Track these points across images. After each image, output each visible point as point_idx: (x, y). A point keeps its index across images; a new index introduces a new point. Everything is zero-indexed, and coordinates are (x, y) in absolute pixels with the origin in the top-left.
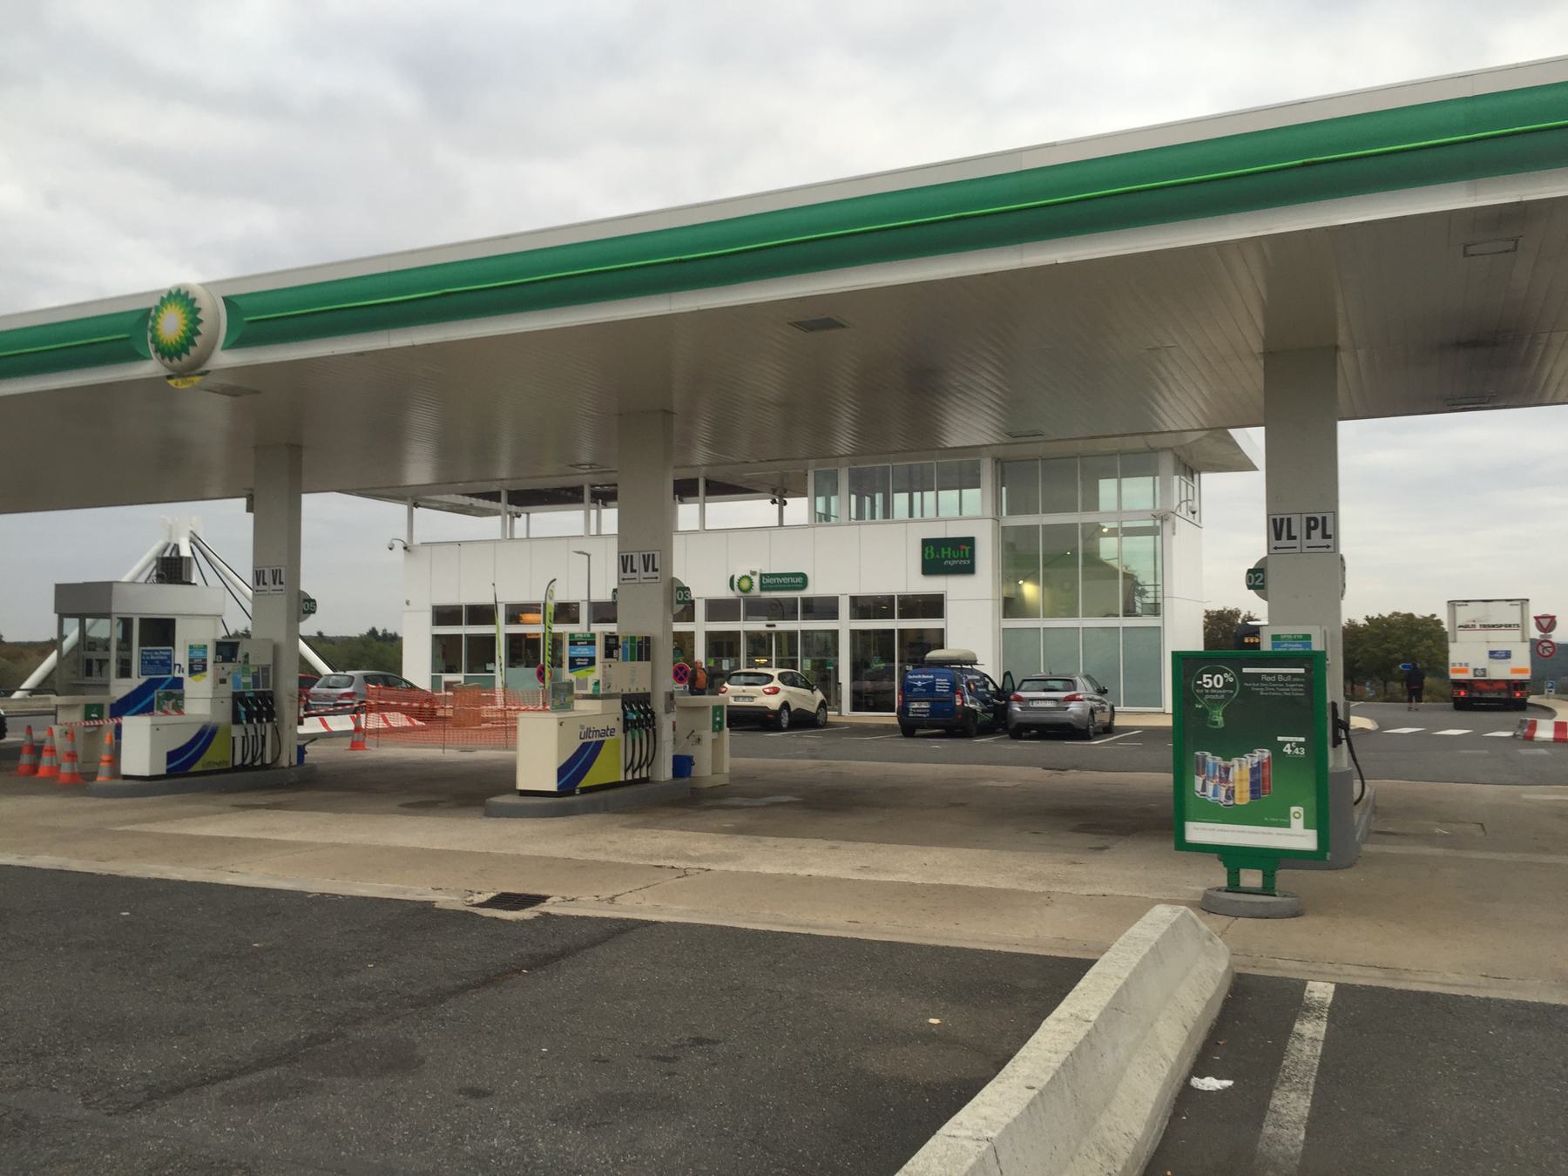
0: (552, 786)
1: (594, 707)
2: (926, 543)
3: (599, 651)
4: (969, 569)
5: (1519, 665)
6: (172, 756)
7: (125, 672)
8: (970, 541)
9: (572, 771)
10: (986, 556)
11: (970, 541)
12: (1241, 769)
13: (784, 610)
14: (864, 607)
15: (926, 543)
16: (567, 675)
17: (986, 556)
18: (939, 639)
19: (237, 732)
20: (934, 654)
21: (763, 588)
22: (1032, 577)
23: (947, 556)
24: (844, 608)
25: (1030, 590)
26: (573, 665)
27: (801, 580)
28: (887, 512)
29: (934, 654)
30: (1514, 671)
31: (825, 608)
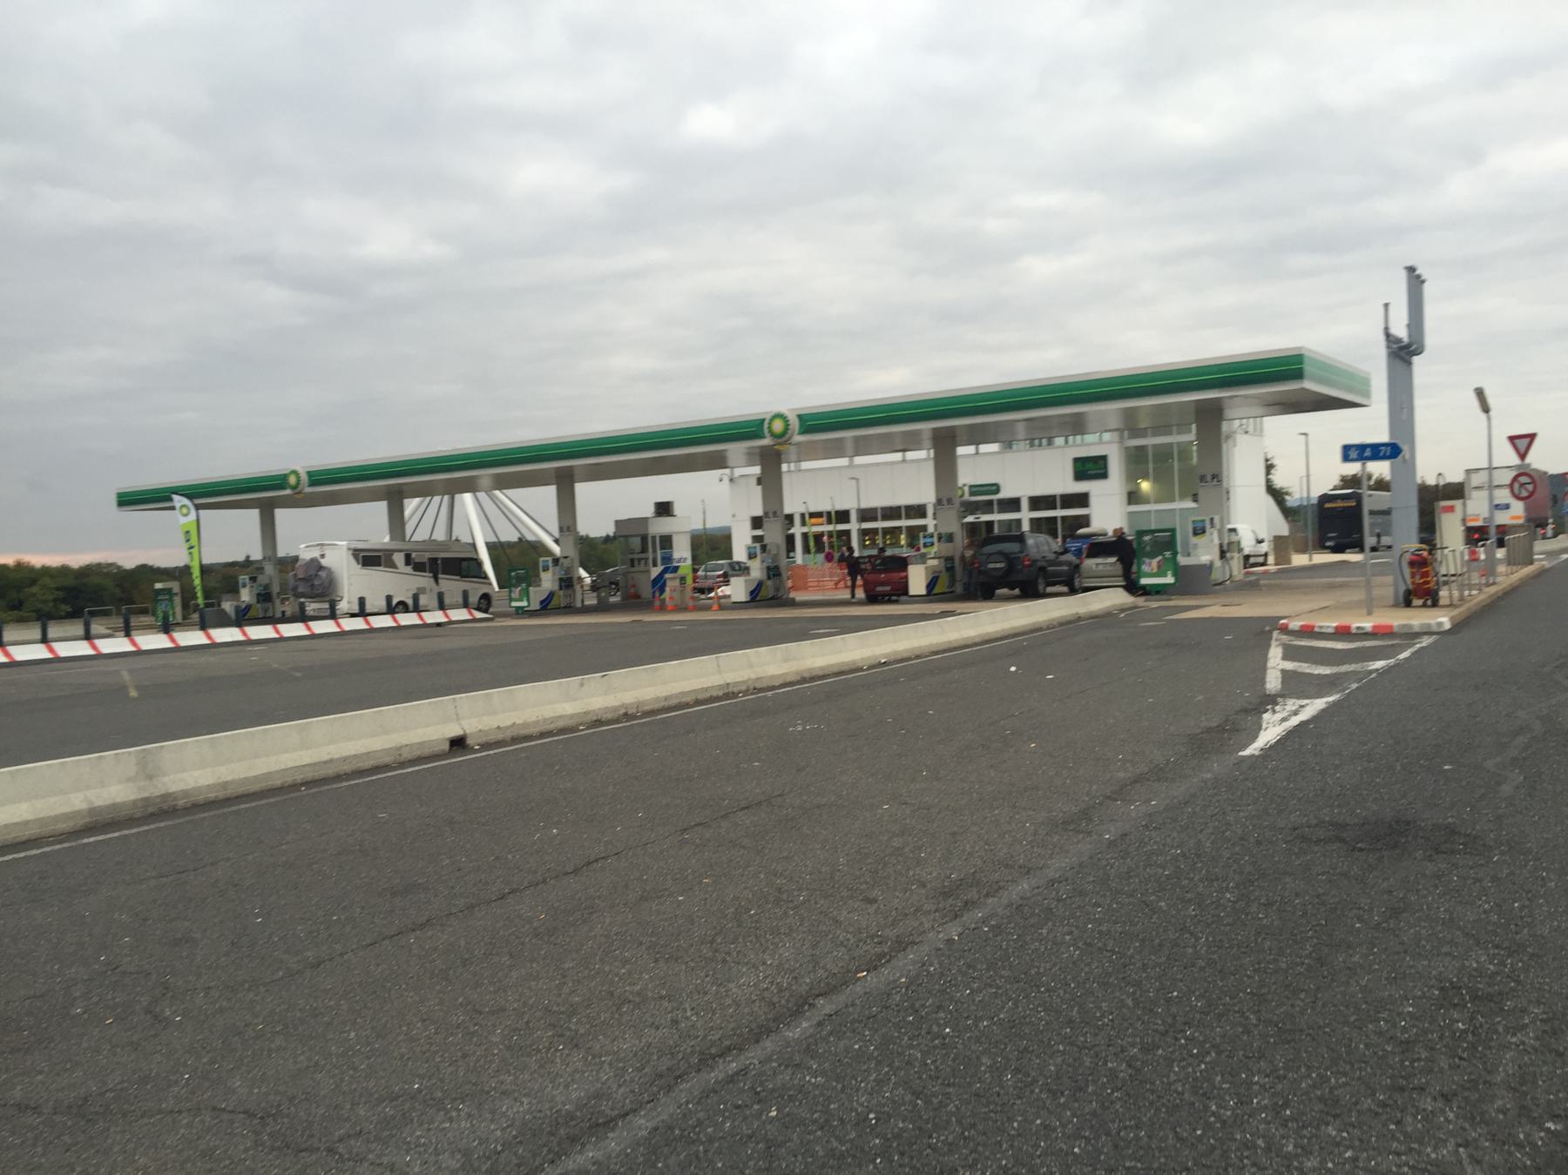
0: (924, 592)
1: (935, 562)
2: (1076, 460)
3: (935, 539)
4: (1103, 475)
5: (1516, 512)
6: (752, 593)
7: (655, 565)
8: (1104, 458)
9: (931, 586)
10: (1116, 467)
11: (1104, 458)
12: (1155, 562)
13: (988, 507)
14: (1037, 502)
15: (1076, 460)
16: (923, 550)
17: (1116, 467)
18: (1084, 521)
19: (769, 583)
20: (1081, 531)
21: (972, 494)
22: (1145, 477)
23: (1090, 468)
24: (1025, 504)
25: (1145, 486)
26: (925, 546)
27: (995, 488)
28: (1050, 443)
29: (1081, 531)
30: (1514, 518)
31: (1013, 504)
